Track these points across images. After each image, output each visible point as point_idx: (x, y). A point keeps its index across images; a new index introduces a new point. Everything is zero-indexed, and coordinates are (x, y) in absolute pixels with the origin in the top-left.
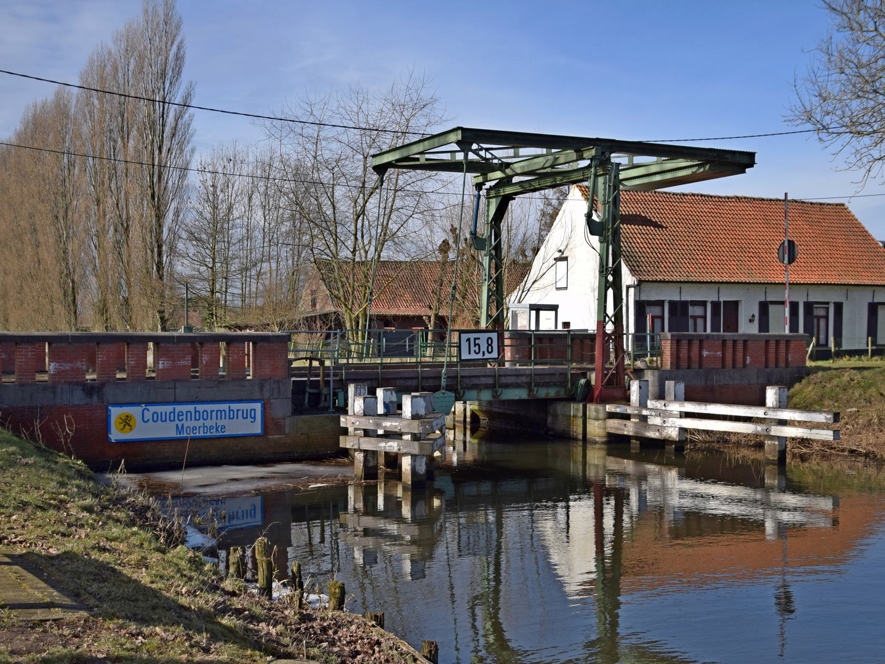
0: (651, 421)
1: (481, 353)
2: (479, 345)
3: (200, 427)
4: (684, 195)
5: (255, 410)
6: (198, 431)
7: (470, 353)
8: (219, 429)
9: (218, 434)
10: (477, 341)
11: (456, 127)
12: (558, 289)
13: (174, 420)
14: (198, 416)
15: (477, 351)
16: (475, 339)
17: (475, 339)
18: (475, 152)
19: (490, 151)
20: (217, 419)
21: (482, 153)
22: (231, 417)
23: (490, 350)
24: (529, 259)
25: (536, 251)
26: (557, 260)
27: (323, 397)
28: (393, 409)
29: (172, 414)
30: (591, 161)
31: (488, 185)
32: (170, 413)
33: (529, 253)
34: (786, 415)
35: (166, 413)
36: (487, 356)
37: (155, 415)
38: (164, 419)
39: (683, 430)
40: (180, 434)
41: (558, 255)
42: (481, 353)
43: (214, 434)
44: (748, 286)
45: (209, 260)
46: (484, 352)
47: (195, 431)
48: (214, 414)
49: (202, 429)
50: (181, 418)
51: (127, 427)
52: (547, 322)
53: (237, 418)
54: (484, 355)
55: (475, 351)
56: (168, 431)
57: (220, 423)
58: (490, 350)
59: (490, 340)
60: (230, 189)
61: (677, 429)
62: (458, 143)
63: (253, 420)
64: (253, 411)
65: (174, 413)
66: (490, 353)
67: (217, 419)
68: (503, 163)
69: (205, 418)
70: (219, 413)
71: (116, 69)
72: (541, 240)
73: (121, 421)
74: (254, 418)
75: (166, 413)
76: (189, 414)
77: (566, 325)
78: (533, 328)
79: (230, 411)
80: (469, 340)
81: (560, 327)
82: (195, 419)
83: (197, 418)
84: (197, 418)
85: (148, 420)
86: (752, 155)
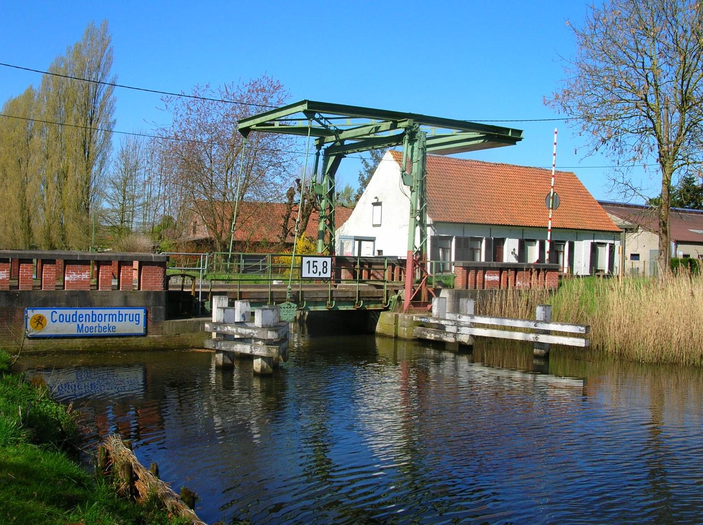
0: (448, 329)
2: (316, 266)
4: (466, 161)
6: (94, 330)
7: (309, 273)
8: (111, 329)
9: (110, 333)
10: (315, 264)
12: (374, 226)
13: (76, 321)
14: (94, 318)
15: (315, 272)
16: (314, 262)
17: (314, 262)
18: (318, 120)
19: (329, 120)
21: (323, 121)
22: (121, 320)
23: (325, 271)
24: (353, 203)
25: (357, 198)
26: (374, 204)
27: (194, 305)
28: (248, 318)
29: (74, 316)
30: (405, 130)
31: (326, 146)
32: (74, 315)
33: (353, 199)
34: (552, 327)
36: (323, 275)
37: (61, 316)
38: (68, 320)
39: (474, 337)
41: (375, 201)
43: (107, 333)
44: (510, 228)
45: (121, 198)
46: (320, 272)
48: (107, 317)
49: (97, 329)
51: (39, 325)
52: (367, 251)
54: (320, 275)
56: (70, 328)
57: (112, 324)
58: (325, 271)
59: (325, 263)
60: (137, 150)
62: (305, 112)
63: (137, 322)
64: (137, 316)
65: (76, 315)
68: (337, 130)
69: (100, 320)
70: (111, 316)
71: (574, 462)
72: (361, 193)
74: (139, 321)
76: (87, 316)
77: (380, 252)
78: (356, 255)
79: (93, 315)
80: (309, 262)
81: (376, 254)
82: (92, 321)
83: (94, 320)
84: (94, 320)
85: (56, 320)
86: (520, 132)
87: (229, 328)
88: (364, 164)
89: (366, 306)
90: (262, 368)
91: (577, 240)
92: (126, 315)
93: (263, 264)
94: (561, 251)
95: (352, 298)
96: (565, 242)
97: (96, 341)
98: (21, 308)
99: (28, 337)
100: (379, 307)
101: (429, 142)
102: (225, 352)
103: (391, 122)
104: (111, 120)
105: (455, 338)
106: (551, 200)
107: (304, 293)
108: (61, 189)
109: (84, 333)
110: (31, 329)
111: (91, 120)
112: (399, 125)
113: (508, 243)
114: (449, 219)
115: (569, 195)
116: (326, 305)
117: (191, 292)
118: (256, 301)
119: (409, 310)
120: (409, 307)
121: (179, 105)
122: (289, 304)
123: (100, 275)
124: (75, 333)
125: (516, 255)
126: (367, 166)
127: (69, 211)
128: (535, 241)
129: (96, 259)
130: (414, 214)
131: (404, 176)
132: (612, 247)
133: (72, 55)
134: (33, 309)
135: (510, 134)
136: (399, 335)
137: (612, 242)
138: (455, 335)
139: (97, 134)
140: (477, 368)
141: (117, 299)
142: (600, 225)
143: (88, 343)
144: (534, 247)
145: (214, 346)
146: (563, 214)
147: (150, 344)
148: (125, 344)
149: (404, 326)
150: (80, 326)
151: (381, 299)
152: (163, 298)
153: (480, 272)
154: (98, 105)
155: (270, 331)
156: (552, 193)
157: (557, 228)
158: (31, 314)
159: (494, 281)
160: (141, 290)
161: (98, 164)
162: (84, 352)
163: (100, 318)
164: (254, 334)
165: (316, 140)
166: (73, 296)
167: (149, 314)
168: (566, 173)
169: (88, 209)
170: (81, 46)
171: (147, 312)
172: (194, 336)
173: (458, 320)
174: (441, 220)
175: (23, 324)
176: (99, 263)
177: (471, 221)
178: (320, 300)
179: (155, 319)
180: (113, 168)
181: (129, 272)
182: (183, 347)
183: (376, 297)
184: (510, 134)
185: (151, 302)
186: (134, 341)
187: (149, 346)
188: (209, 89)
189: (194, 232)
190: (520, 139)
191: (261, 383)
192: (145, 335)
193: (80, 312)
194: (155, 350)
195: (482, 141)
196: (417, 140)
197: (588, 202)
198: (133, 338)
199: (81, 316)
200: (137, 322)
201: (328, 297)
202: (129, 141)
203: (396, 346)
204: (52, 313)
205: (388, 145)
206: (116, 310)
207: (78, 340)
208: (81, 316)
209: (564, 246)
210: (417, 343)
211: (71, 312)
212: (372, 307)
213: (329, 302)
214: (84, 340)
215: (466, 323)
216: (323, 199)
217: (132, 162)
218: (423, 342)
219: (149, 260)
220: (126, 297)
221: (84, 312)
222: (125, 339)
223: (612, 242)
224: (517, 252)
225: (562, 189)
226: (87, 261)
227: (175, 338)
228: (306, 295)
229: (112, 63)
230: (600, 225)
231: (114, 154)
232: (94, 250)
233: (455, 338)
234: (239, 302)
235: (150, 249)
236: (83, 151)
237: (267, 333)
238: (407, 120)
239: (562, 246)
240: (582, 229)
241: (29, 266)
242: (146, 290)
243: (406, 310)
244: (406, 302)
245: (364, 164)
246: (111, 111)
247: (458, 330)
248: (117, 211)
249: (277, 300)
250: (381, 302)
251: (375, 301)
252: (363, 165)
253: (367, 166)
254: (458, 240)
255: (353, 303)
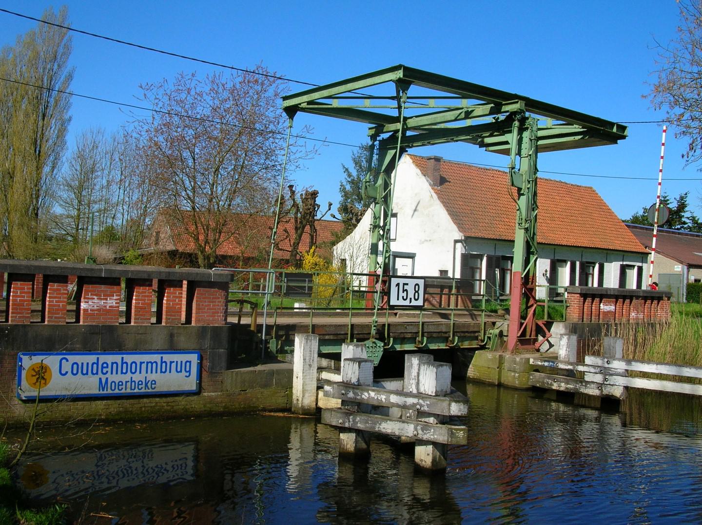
0: (588, 378)
1: (408, 299)
2: (406, 290)
3: (126, 382)
5: (190, 362)
7: (398, 299)
8: (149, 385)
9: (147, 390)
11: (397, 64)
13: (97, 373)
15: (405, 298)
16: (404, 284)
17: (404, 284)
20: (147, 373)
22: (164, 370)
23: (416, 298)
29: (95, 366)
32: (93, 364)
35: (88, 364)
36: (414, 303)
37: (75, 366)
38: (85, 372)
40: (103, 390)
42: (408, 299)
43: (143, 390)
44: (543, 246)
45: (76, 202)
46: (411, 299)
47: (140, 387)
48: (144, 366)
49: (129, 384)
50: (105, 370)
53: (170, 372)
54: (410, 302)
55: (403, 297)
56: (89, 385)
57: (152, 377)
61: (622, 388)
63: (188, 374)
66: (416, 300)
67: (147, 373)
69: (133, 371)
70: (150, 365)
73: (35, 374)
74: (190, 371)
75: (88, 364)
76: (115, 365)
79: (123, 363)
80: (398, 285)
83: (124, 371)
85: (67, 372)
87: (372, 394)
88: (346, 173)
89: (460, 344)
90: (434, 460)
91: (607, 262)
92: (171, 363)
93: (310, 285)
94: (508, 270)
95: (446, 333)
96: (594, 263)
97: (127, 403)
98: (12, 352)
99: (22, 401)
100: (474, 345)
101: (541, 134)
102: (358, 432)
103: (492, 105)
104: (66, 117)
105: (601, 390)
106: (656, 213)
107: (391, 328)
108: (5, 191)
109: (110, 391)
110: (27, 389)
111: (44, 116)
112: (505, 108)
113: (540, 263)
114: (480, 235)
115: (593, 212)
116: (415, 343)
117: (249, 326)
118: (332, 337)
119: (516, 349)
120: (516, 345)
121: (160, 94)
122: (374, 343)
123: (134, 301)
124: (95, 391)
125: (547, 277)
126: (350, 175)
127: (16, 217)
128: (565, 261)
129: (130, 276)
130: (523, 224)
131: (513, 173)
132: (640, 269)
133: (23, 45)
134: (31, 355)
135: (615, 130)
136: (502, 382)
137: (640, 264)
138: (600, 386)
139: (49, 131)
140: (638, 434)
141: (159, 338)
142: (628, 246)
143: (114, 407)
144: (564, 269)
145: (341, 421)
146: (591, 233)
147: (205, 406)
148: (169, 408)
149: (515, 372)
150: (104, 381)
151: (477, 334)
152: (224, 337)
153: (597, 300)
154: (52, 99)
155: (456, 402)
156: (658, 204)
157: (589, 247)
158: (28, 362)
159: (609, 312)
160: (193, 324)
161: (50, 164)
162: (108, 421)
163: (134, 368)
164: (421, 406)
165: (370, 129)
166: (93, 334)
167: (204, 361)
168: (586, 187)
169: (37, 214)
170: (35, 33)
171: (201, 358)
172: (266, 392)
173: (606, 365)
174: (473, 235)
175: (13, 379)
176: (133, 283)
177: (504, 238)
178: (409, 336)
179: (212, 368)
180: (66, 170)
181: (177, 297)
182: (250, 413)
183: (471, 332)
184: (615, 130)
185: (207, 343)
186: (182, 401)
187: (203, 409)
188: (195, 78)
189: (157, 243)
190: (624, 137)
191: (432, 489)
192: (198, 392)
193: (104, 358)
194: (211, 416)
195: (580, 137)
196: (527, 128)
197: (612, 220)
198: (180, 398)
199: (105, 365)
200: (188, 374)
201: (419, 332)
202: (87, 140)
203: (499, 394)
204: (61, 361)
205: (428, 143)
206: (156, 355)
207: (99, 402)
208: (153, 382)
209: (594, 268)
210: (530, 394)
211: (91, 359)
212: (466, 345)
213: (419, 339)
214: (109, 402)
215: (619, 370)
216: (523, 194)
217: (90, 162)
218: (539, 392)
219: (207, 280)
220: (172, 336)
221: (109, 359)
222: (169, 399)
223: (640, 264)
224: (548, 275)
225: (585, 205)
226: (116, 278)
227: (238, 397)
228: (392, 329)
229: (70, 53)
230: (628, 246)
231: (69, 153)
232: (92, 261)
233: (601, 390)
234: (351, 347)
235: (111, 260)
236: (33, 149)
237: (450, 405)
238: (517, 102)
239: (591, 267)
240: (612, 250)
241: (27, 286)
242: (200, 325)
243: (513, 350)
244: (512, 339)
245: (346, 173)
246: (67, 106)
247: (605, 379)
248: (72, 217)
249: (358, 336)
250: (476, 338)
251: (470, 337)
252: (345, 175)
253: (350, 175)
254: (489, 259)
255: (446, 340)
